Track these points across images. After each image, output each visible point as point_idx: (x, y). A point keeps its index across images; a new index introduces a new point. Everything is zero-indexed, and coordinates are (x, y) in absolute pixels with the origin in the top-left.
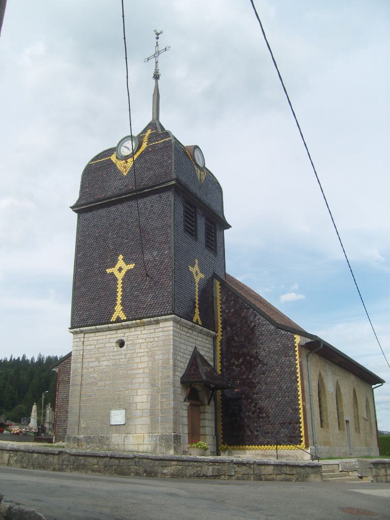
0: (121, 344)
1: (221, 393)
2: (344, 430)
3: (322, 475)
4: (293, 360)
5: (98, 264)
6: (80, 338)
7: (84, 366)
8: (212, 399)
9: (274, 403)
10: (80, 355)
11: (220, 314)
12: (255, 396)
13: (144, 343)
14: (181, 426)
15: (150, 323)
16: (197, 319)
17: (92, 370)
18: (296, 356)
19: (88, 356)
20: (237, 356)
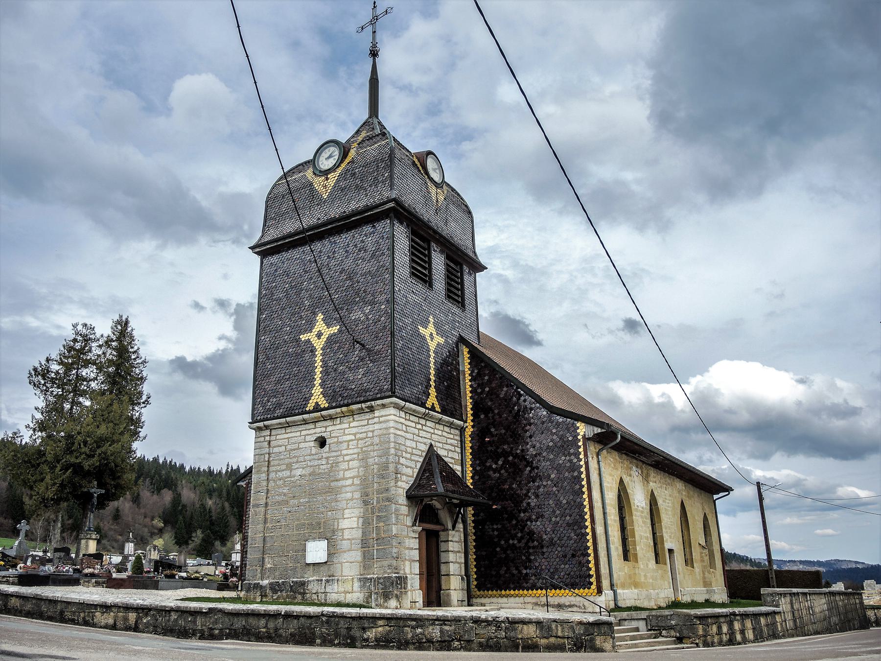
0: (322, 442)
1: (473, 512)
2: (666, 564)
3: (613, 638)
4: (575, 460)
5: (288, 328)
6: (264, 436)
7: (270, 477)
8: (460, 520)
9: (550, 526)
10: (265, 461)
11: (470, 395)
12: (522, 515)
13: (352, 440)
14: (407, 563)
15: (361, 411)
16: (433, 404)
17: (281, 482)
18: (580, 453)
19: (276, 462)
20: (496, 457)
